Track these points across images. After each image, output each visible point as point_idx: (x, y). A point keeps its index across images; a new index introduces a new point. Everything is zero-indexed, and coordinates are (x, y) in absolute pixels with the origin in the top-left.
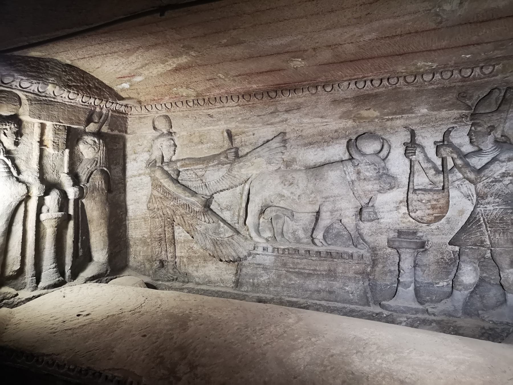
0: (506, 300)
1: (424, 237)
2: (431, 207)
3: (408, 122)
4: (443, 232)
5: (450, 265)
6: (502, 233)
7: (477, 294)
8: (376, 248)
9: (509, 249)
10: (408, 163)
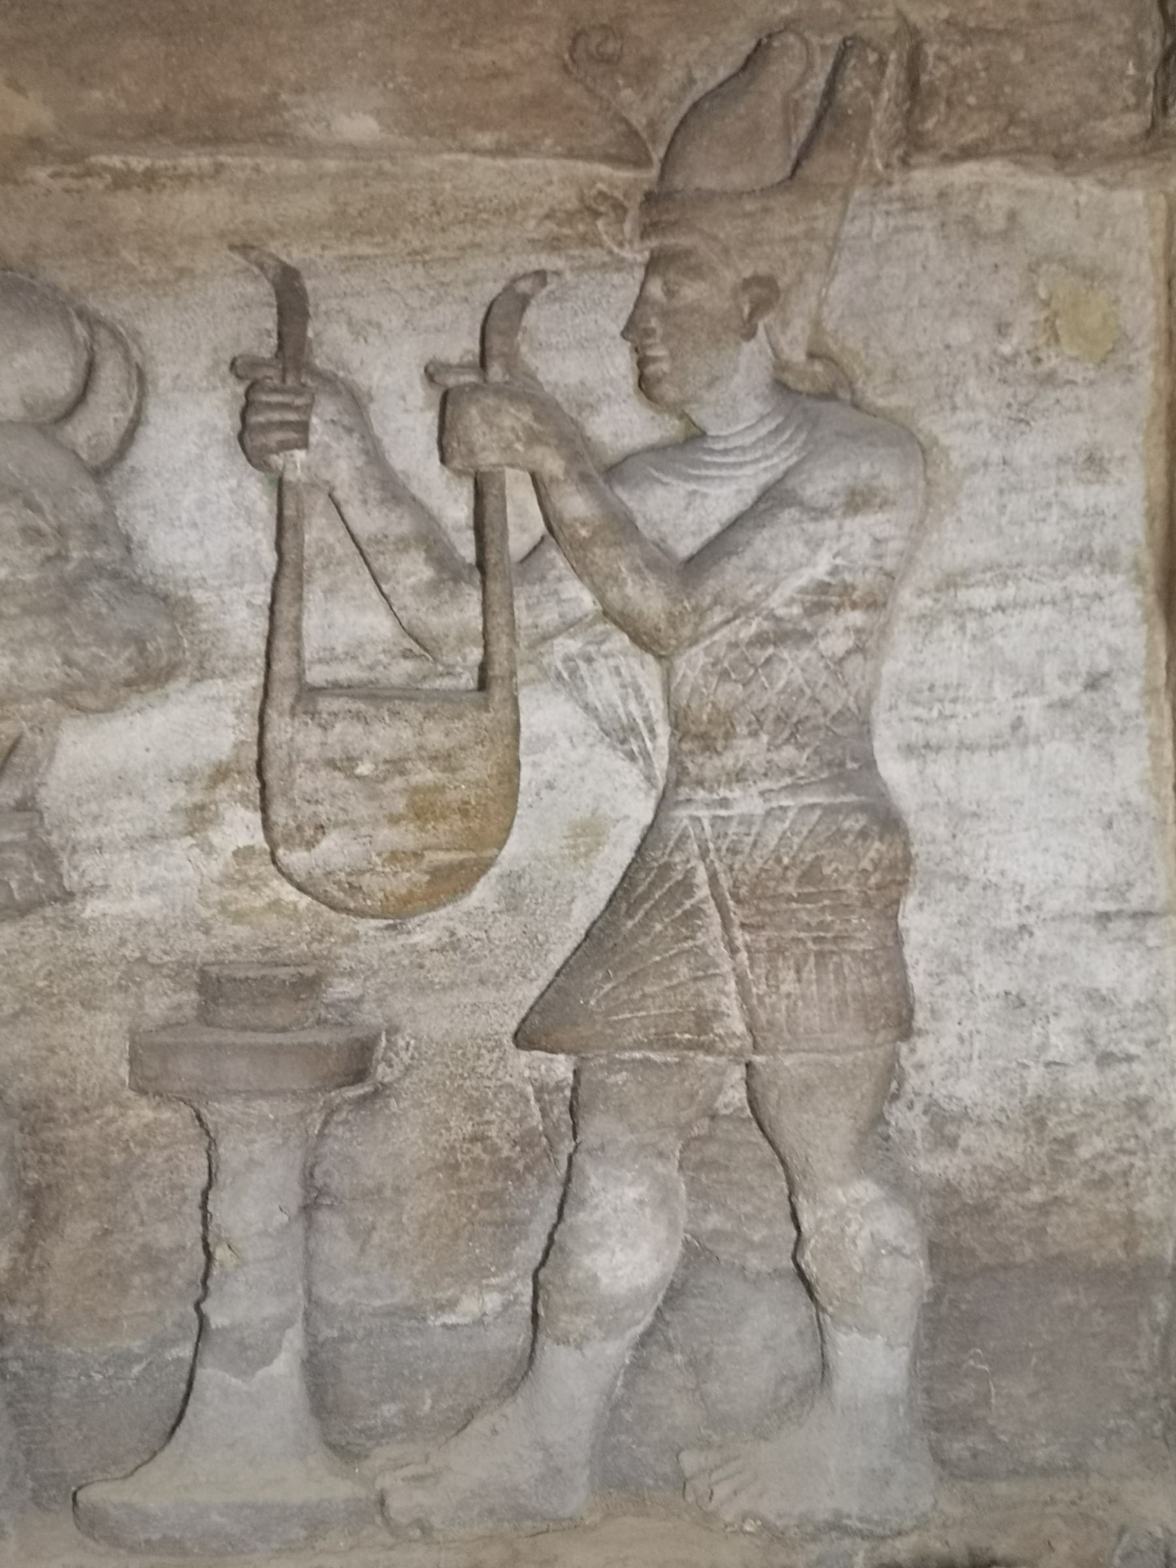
0: (824, 1368)
1: (366, 1007)
2: (411, 805)
3: (257, 211)
4: (484, 965)
5: (519, 1178)
6: (812, 960)
7: (670, 1348)
8: (50, 1105)
9: (849, 1058)
10: (263, 504)
